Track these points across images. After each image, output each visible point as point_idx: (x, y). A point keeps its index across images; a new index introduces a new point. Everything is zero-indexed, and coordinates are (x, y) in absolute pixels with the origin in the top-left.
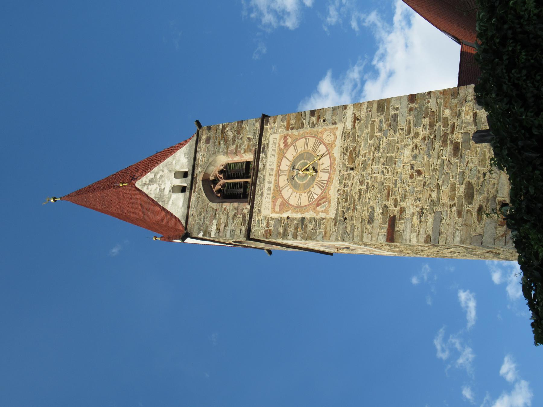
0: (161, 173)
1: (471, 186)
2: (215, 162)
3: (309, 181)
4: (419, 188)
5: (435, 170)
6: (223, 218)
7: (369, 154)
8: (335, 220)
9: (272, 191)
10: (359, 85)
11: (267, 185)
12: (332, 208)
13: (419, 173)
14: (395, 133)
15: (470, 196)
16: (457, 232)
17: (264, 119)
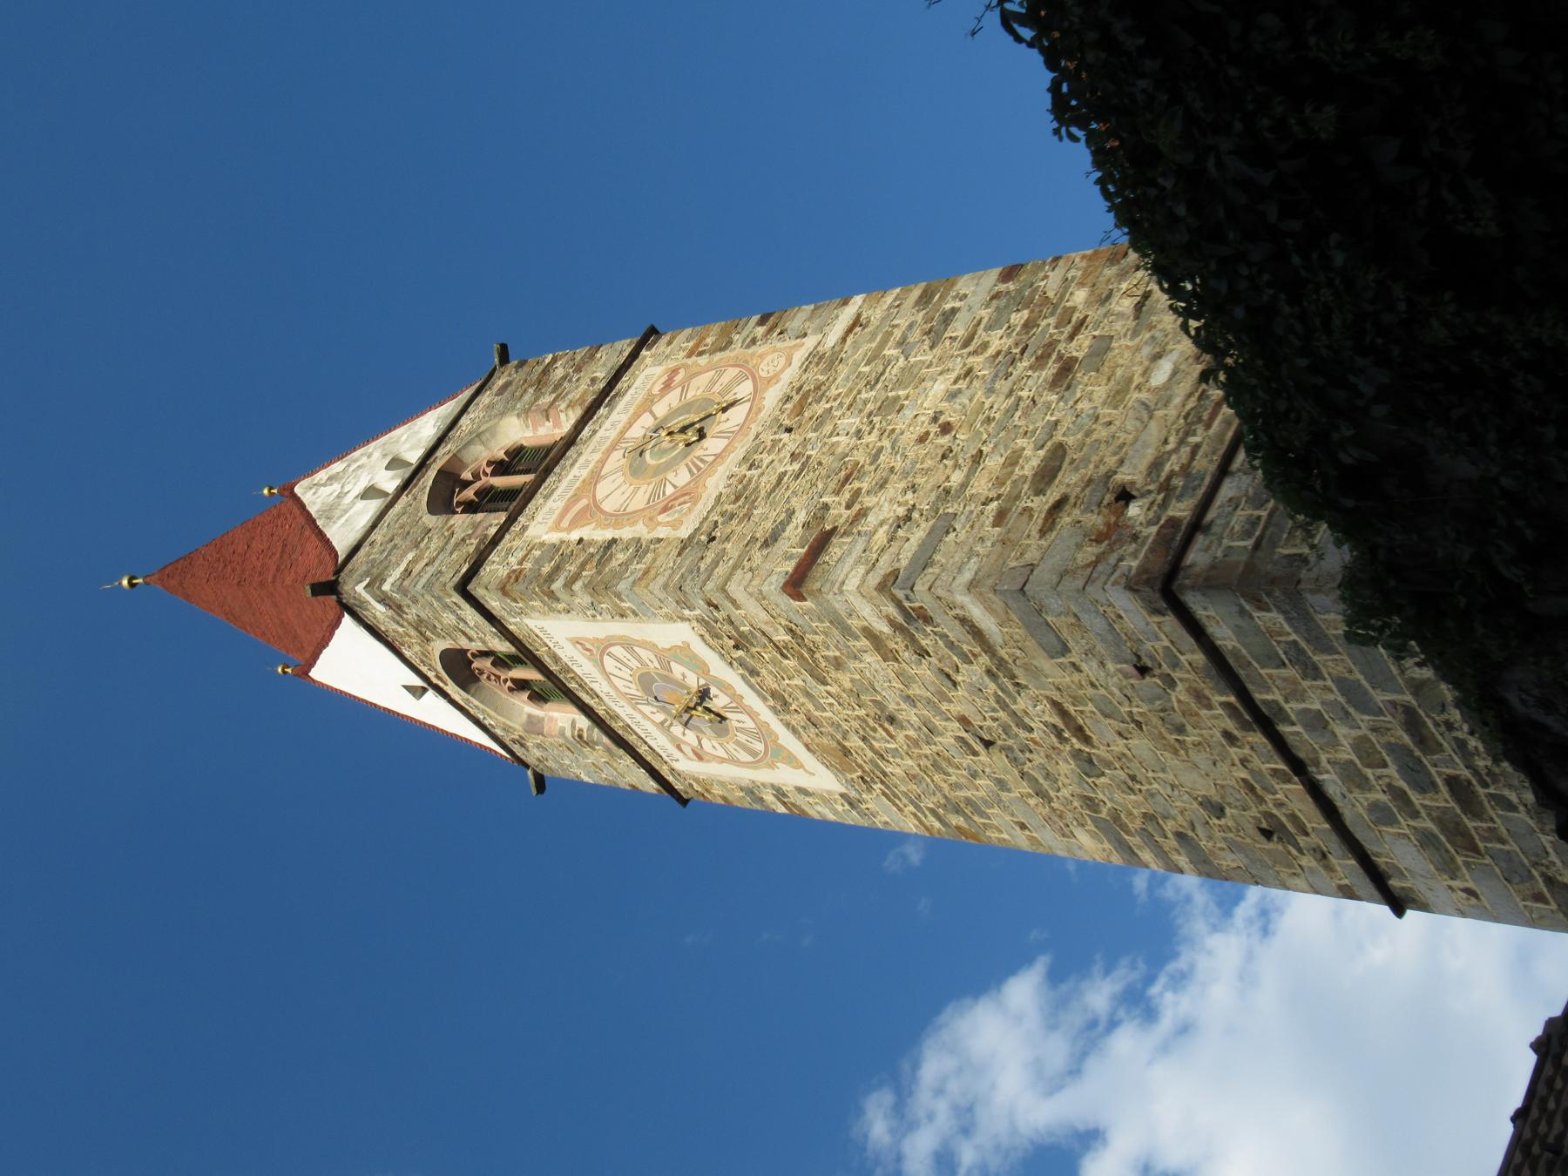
0: (364, 460)
1: (1060, 453)
2: (494, 435)
3: (675, 458)
4: (929, 463)
5: (989, 420)
6: (433, 546)
7: (847, 395)
8: (685, 545)
9: (578, 484)
10: (1101, 1028)
11: (575, 471)
12: (692, 516)
13: (946, 428)
14: (931, 348)
15: (1046, 476)
16: (974, 559)
17: (650, 336)
